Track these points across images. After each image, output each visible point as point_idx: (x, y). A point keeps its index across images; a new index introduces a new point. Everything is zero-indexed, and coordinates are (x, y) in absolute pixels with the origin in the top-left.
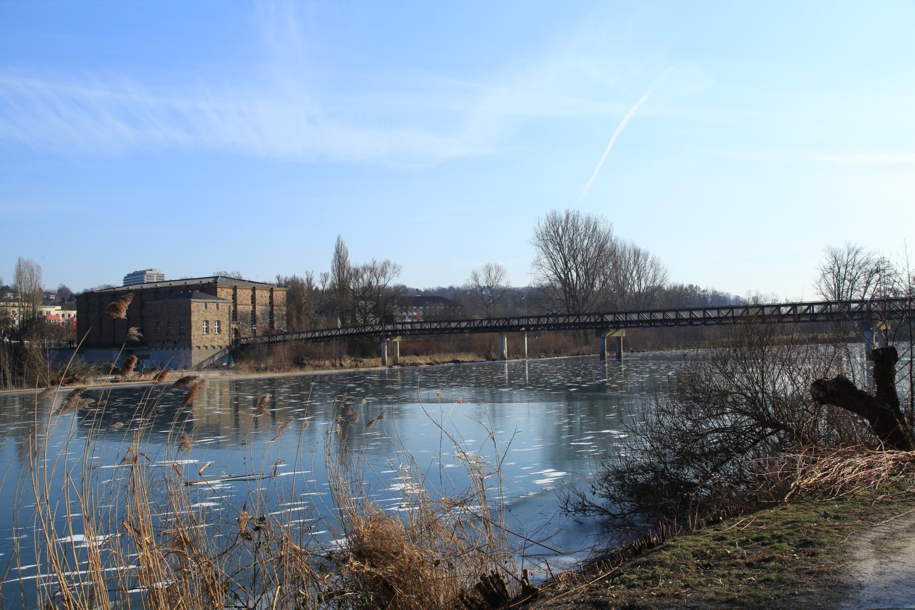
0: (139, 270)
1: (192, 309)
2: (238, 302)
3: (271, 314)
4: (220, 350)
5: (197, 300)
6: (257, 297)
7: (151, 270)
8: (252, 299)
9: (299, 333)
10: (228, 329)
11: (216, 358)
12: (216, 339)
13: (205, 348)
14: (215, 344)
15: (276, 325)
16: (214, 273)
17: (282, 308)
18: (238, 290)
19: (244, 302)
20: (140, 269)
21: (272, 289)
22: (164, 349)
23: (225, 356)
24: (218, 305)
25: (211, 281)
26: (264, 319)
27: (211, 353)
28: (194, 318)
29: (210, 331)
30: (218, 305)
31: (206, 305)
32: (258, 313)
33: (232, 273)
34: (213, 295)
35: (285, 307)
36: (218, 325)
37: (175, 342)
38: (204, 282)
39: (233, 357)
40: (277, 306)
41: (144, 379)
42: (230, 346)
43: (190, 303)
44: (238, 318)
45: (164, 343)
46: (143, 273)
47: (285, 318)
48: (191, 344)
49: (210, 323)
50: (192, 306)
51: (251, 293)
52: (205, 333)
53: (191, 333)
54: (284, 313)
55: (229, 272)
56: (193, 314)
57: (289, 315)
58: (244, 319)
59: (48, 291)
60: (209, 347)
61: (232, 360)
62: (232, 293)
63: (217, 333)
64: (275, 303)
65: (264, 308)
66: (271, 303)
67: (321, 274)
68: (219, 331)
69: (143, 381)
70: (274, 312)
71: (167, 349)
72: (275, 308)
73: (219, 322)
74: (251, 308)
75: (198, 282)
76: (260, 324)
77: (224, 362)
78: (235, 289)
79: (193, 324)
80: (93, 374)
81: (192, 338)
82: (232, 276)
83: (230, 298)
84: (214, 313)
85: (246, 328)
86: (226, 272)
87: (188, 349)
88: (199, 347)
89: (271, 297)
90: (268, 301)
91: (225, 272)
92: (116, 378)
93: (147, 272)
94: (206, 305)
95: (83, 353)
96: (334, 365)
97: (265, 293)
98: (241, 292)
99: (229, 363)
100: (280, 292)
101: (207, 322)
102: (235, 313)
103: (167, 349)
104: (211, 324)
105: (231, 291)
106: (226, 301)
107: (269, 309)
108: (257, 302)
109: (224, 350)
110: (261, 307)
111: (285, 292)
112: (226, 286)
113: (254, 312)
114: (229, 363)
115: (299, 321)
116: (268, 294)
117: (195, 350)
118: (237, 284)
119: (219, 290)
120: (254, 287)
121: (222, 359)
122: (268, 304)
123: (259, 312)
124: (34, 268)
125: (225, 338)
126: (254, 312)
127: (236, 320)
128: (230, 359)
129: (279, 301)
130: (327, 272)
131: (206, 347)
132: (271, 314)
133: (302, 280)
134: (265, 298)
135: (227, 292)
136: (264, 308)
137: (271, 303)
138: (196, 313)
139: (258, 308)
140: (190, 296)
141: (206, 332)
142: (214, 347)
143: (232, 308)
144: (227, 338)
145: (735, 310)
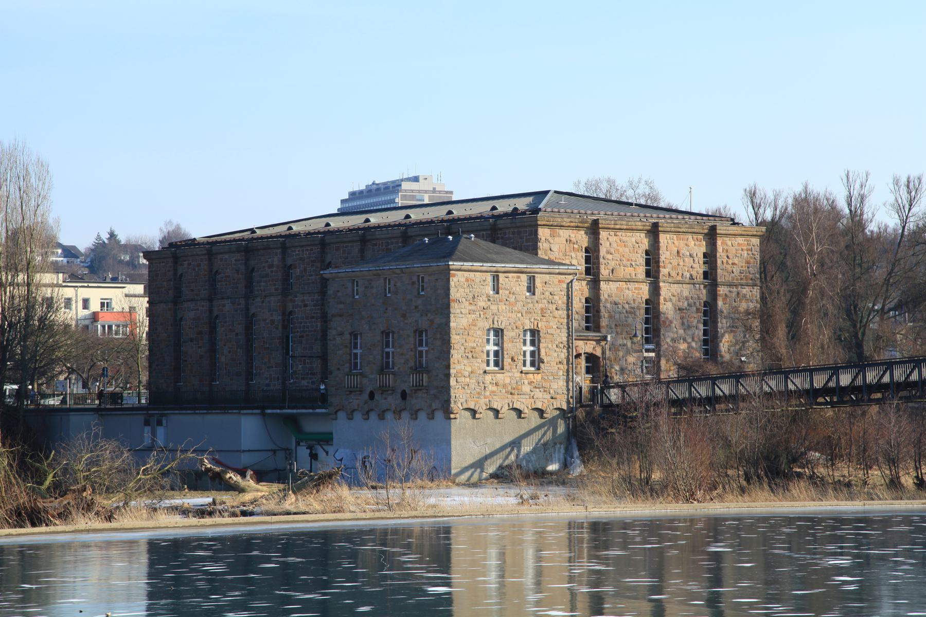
0: (381, 179)
1: (454, 293)
2: (604, 272)
3: (710, 311)
4: (540, 421)
5: (467, 265)
6: (664, 255)
7: (416, 179)
8: (648, 263)
9: (714, 380)
10: (563, 355)
11: (527, 447)
12: (526, 388)
13: (491, 414)
14: (522, 403)
15: (725, 344)
16: (577, 185)
17: (746, 291)
18: (603, 234)
19: (622, 272)
20: (383, 177)
21: (713, 229)
22: (373, 416)
23: (554, 442)
24: (532, 280)
25: (522, 204)
26: (687, 327)
27: (510, 429)
28: (459, 320)
29: (507, 360)
30: (532, 280)
31: (496, 278)
32: (666, 308)
33: (631, 183)
34: (533, 254)
35: (756, 292)
36: (533, 343)
37: (404, 395)
38: (504, 207)
39: (581, 448)
40: (730, 285)
41: (292, 509)
42: (571, 410)
43: (446, 274)
44: (604, 322)
45: (372, 396)
46: (393, 187)
47: (756, 324)
48: (448, 401)
49: (508, 335)
50: (453, 282)
51: (645, 243)
52: (492, 367)
53: (448, 367)
54: (319, 315)
55: (622, 182)
56: (455, 308)
57: (765, 315)
58: (620, 326)
59: (133, 242)
60: (504, 411)
61: (576, 453)
62: (585, 244)
63: (528, 368)
64: (721, 275)
65: (686, 290)
66: (710, 275)
67: (896, 182)
68: (536, 361)
69: (288, 513)
70: (720, 303)
71: (414, 416)
72: (722, 290)
73: (535, 333)
74: (644, 291)
75: (484, 209)
76: (673, 340)
77: (549, 460)
78: (594, 229)
79: (455, 338)
80: (141, 489)
81: (453, 382)
82: (630, 196)
83: (578, 262)
84: (519, 305)
85: (628, 352)
86: (611, 182)
87: (439, 415)
88: (473, 412)
89: (710, 257)
90: (699, 268)
91: (608, 181)
92: (214, 502)
93: (405, 186)
94: (496, 278)
95: (160, 423)
96: (894, 484)
97: (692, 243)
98: (613, 239)
99: (565, 465)
100: (740, 240)
101: (499, 333)
102: (593, 305)
103: (382, 417)
104: (512, 340)
105: (582, 238)
106: (556, 269)
107: (703, 294)
108: (664, 271)
109: (553, 422)
110: (676, 288)
111: (756, 241)
112: (566, 221)
113: (652, 305)
114: (565, 465)
115: (795, 334)
116: (700, 248)
117: (460, 422)
118: (601, 214)
119: (543, 233)
120: (596, 223)
121: (544, 449)
122: (700, 278)
123: (669, 305)
124: (30, 169)
125: (555, 386)
126: (652, 305)
127: (597, 328)
128: (568, 451)
129: (736, 270)
130: (914, 174)
131: (496, 412)
132: (710, 311)
133: (833, 207)
134: (689, 261)
135: (569, 241)
136: (686, 290)
137: (710, 275)
138: (465, 307)
139: (666, 290)
140: (450, 253)
141: (496, 364)
142: (519, 412)
143: (581, 290)
144: (559, 385)
145: (55, 282)
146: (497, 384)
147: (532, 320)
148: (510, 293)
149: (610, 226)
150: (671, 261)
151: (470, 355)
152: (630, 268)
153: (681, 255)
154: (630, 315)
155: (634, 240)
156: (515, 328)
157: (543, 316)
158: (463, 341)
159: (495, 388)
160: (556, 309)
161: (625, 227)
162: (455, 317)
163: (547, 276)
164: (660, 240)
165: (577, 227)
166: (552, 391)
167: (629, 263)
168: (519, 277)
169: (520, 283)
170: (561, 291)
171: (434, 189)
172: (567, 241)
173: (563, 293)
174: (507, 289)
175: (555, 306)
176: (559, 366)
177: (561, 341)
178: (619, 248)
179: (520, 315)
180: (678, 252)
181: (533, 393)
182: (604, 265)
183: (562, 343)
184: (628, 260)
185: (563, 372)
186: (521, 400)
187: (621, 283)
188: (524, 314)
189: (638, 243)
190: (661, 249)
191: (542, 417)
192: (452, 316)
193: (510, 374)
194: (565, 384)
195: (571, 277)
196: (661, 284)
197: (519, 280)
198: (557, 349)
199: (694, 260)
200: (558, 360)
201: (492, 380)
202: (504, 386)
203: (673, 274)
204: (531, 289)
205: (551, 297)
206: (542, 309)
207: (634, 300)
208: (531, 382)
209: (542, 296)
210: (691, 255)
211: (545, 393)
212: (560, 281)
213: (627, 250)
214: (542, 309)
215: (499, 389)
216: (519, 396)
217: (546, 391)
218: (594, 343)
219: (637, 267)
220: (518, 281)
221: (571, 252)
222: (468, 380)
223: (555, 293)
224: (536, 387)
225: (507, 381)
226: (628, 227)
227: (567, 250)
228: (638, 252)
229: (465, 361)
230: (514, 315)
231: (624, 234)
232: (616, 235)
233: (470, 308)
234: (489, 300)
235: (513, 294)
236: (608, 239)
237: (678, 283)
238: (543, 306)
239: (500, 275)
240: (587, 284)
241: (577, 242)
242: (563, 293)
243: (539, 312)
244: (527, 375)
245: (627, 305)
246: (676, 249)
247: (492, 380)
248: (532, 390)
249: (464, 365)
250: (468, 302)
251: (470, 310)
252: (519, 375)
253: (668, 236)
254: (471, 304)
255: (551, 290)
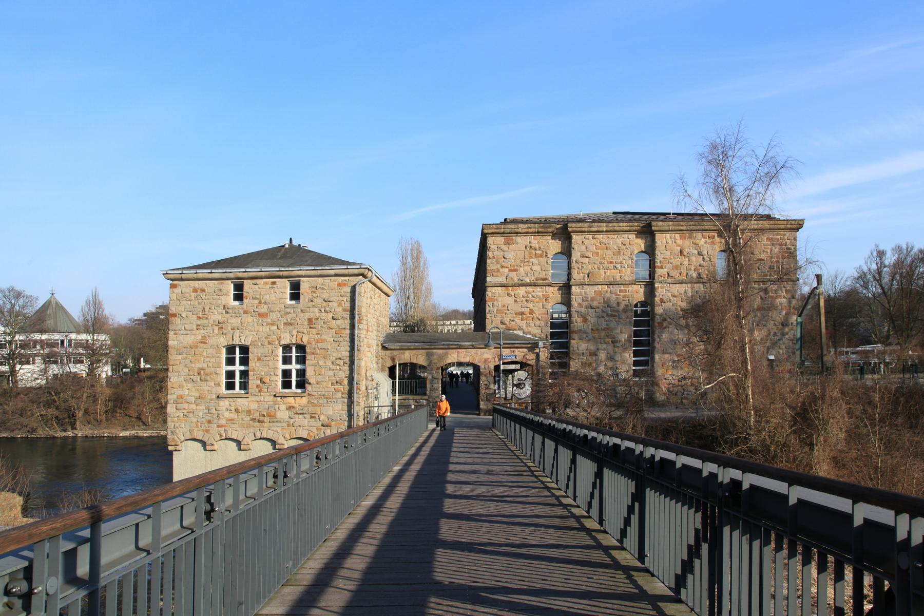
18: (576, 238)
146: (237, 411)
147: (294, 332)
148: (260, 302)
149: (583, 229)
150: (671, 261)
151: (197, 378)
152: (613, 271)
153: (685, 253)
154: (611, 319)
155: (619, 242)
156: (266, 343)
157: (310, 328)
158: (188, 362)
159: (234, 416)
160: (333, 318)
161: (604, 229)
162: (175, 334)
163: (320, 279)
164: (656, 240)
165: (538, 232)
166: (322, 417)
167: (612, 265)
168: (274, 283)
169: (276, 290)
170: (341, 296)
171: (505, 220)
172: (526, 248)
173: (345, 299)
174: (256, 298)
175: (331, 315)
176: (336, 387)
177: (339, 356)
178: (599, 251)
179: (275, 327)
180: (681, 251)
181: (293, 420)
182: (577, 270)
183: (340, 359)
184: (611, 263)
185: (343, 393)
186: (275, 429)
187: (600, 286)
188: (281, 327)
189: (624, 245)
190: (657, 249)
191: (274, 448)
192: (171, 333)
193: (258, 398)
194: (346, 408)
195: (354, 280)
196: (656, 285)
197: (275, 286)
198: (334, 367)
199: (703, 258)
200: (335, 380)
201: (230, 405)
202: (249, 412)
203: (674, 273)
204: (295, 296)
205: (324, 304)
206: (310, 320)
207: (618, 303)
208: (290, 407)
209: (310, 304)
210: (700, 254)
211: (313, 420)
212: (339, 285)
213: (610, 252)
214: (310, 320)
215: (240, 417)
216: (271, 424)
217: (314, 417)
218: (526, 350)
219: (623, 269)
220: (272, 288)
221: (532, 258)
222: (193, 406)
223: (331, 299)
224: (297, 413)
225: (254, 406)
226: (608, 229)
227: (526, 257)
228: (625, 253)
229: (188, 385)
230: (266, 329)
231: (605, 237)
232: (593, 238)
233: (199, 323)
234: (227, 313)
235: (265, 303)
236: (583, 242)
237: (681, 282)
238: (312, 315)
239: (246, 282)
240: (559, 290)
241: (540, 248)
242: (345, 299)
243: (306, 323)
244: (285, 399)
245: (609, 309)
246: (679, 248)
247: (230, 405)
248: (292, 416)
249: (188, 389)
250: (195, 317)
251: (198, 325)
252: (272, 398)
253: (668, 236)
254: (200, 318)
255: (325, 295)
